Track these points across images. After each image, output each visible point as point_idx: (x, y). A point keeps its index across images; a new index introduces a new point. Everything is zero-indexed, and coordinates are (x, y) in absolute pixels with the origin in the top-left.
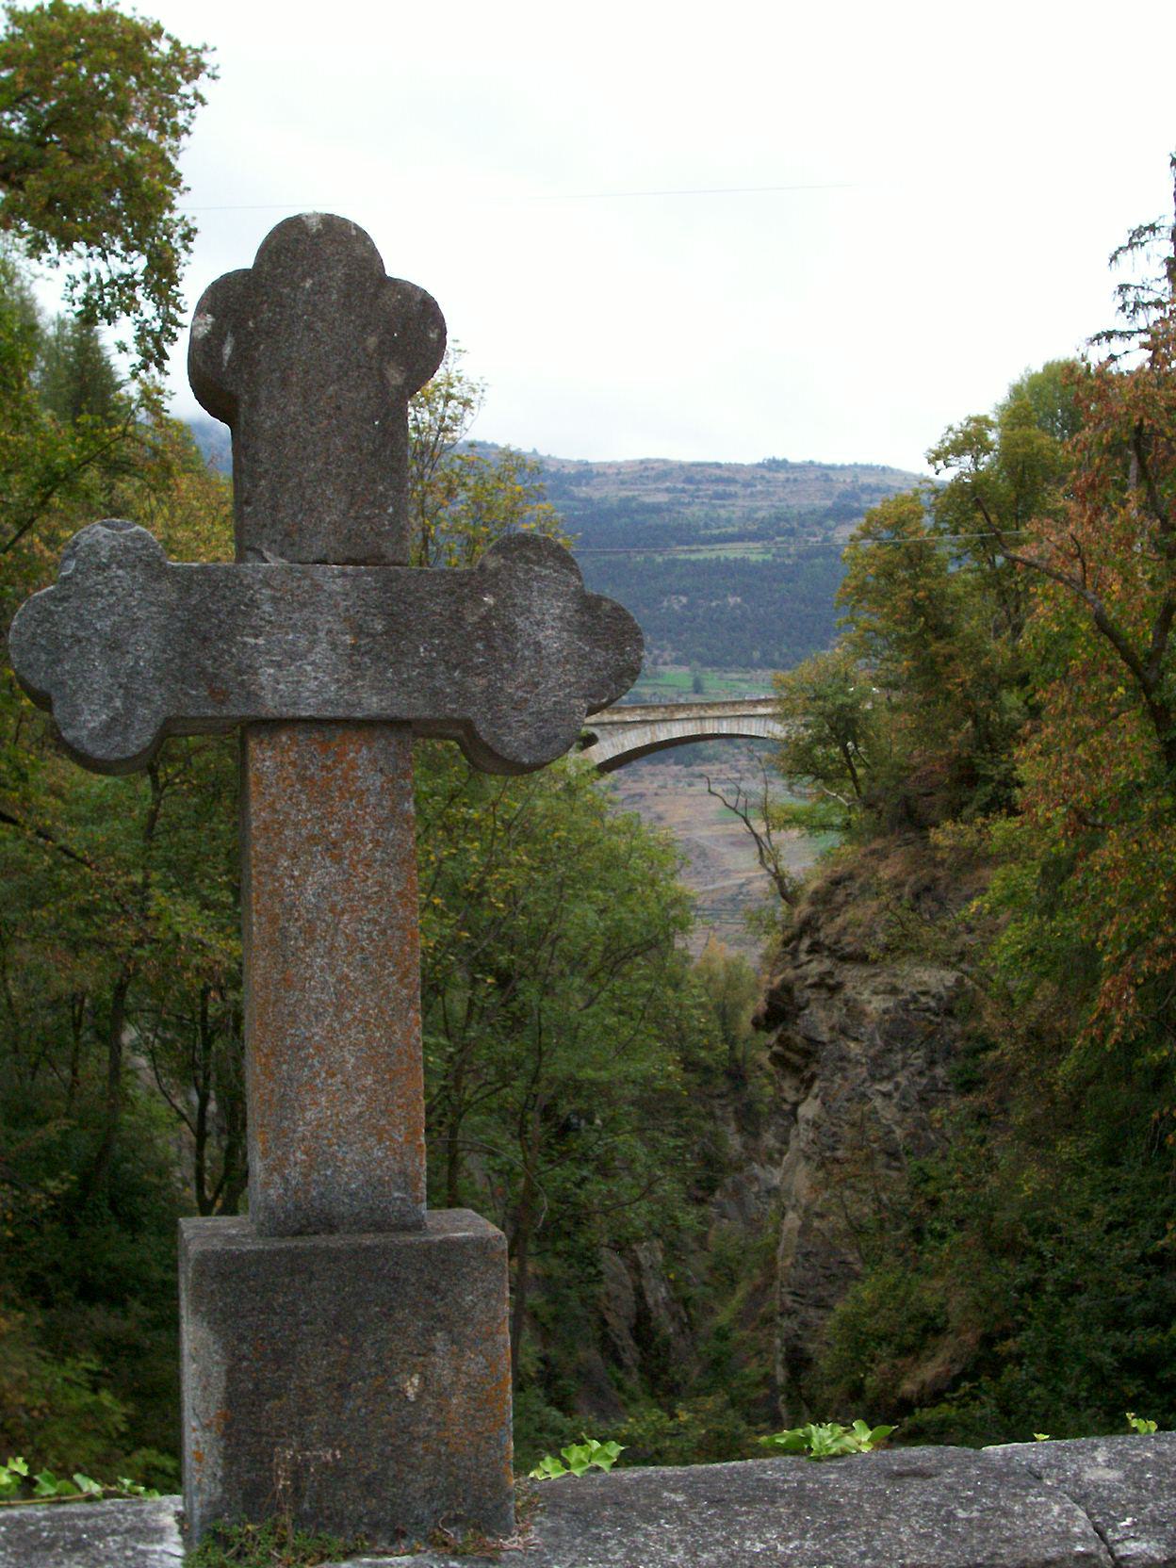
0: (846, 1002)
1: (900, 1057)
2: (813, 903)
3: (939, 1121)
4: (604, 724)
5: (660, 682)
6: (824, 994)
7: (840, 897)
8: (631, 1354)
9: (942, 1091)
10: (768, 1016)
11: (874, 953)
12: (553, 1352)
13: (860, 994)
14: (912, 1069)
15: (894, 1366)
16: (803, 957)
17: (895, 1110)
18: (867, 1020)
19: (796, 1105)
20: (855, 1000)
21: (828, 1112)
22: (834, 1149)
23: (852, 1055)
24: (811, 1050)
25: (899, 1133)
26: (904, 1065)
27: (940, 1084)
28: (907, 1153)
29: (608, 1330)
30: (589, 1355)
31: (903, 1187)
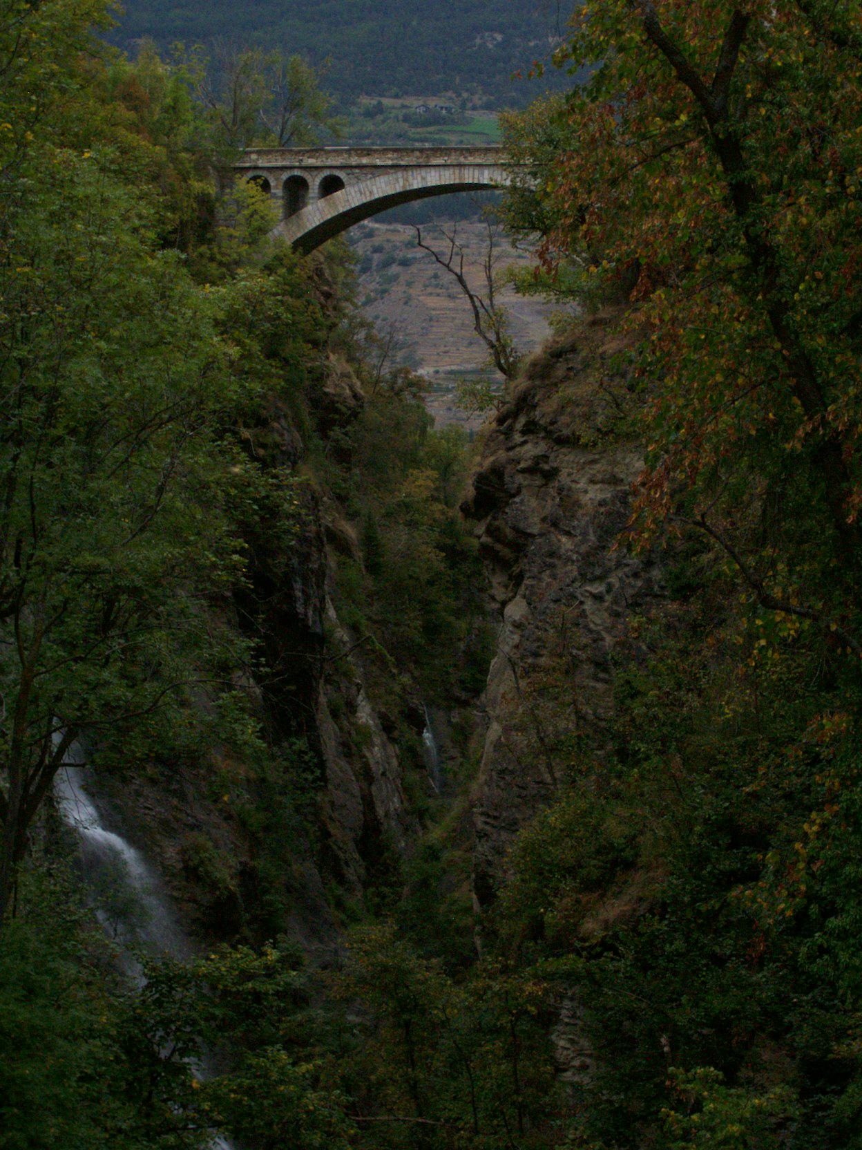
2: (531, 378)
4: (351, 167)
5: (469, 129)
6: (538, 480)
8: (354, 871)
9: (656, 596)
10: (477, 501)
11: (586, 437)
12: (259, 864)
14: (626, 569)
15: (578, 901)
16: (518, 438)
18: (580, 512)
19: (504, 604)
20: (570, 489)
22: (536, 655)
23: (563, 551)
24: (520, 542)
25: (609, 640)
26: (619, 565)
27: (656, 588)
28: (616, 664)
29: (330, 842)
30: (305, 869)
31: (610, 701)
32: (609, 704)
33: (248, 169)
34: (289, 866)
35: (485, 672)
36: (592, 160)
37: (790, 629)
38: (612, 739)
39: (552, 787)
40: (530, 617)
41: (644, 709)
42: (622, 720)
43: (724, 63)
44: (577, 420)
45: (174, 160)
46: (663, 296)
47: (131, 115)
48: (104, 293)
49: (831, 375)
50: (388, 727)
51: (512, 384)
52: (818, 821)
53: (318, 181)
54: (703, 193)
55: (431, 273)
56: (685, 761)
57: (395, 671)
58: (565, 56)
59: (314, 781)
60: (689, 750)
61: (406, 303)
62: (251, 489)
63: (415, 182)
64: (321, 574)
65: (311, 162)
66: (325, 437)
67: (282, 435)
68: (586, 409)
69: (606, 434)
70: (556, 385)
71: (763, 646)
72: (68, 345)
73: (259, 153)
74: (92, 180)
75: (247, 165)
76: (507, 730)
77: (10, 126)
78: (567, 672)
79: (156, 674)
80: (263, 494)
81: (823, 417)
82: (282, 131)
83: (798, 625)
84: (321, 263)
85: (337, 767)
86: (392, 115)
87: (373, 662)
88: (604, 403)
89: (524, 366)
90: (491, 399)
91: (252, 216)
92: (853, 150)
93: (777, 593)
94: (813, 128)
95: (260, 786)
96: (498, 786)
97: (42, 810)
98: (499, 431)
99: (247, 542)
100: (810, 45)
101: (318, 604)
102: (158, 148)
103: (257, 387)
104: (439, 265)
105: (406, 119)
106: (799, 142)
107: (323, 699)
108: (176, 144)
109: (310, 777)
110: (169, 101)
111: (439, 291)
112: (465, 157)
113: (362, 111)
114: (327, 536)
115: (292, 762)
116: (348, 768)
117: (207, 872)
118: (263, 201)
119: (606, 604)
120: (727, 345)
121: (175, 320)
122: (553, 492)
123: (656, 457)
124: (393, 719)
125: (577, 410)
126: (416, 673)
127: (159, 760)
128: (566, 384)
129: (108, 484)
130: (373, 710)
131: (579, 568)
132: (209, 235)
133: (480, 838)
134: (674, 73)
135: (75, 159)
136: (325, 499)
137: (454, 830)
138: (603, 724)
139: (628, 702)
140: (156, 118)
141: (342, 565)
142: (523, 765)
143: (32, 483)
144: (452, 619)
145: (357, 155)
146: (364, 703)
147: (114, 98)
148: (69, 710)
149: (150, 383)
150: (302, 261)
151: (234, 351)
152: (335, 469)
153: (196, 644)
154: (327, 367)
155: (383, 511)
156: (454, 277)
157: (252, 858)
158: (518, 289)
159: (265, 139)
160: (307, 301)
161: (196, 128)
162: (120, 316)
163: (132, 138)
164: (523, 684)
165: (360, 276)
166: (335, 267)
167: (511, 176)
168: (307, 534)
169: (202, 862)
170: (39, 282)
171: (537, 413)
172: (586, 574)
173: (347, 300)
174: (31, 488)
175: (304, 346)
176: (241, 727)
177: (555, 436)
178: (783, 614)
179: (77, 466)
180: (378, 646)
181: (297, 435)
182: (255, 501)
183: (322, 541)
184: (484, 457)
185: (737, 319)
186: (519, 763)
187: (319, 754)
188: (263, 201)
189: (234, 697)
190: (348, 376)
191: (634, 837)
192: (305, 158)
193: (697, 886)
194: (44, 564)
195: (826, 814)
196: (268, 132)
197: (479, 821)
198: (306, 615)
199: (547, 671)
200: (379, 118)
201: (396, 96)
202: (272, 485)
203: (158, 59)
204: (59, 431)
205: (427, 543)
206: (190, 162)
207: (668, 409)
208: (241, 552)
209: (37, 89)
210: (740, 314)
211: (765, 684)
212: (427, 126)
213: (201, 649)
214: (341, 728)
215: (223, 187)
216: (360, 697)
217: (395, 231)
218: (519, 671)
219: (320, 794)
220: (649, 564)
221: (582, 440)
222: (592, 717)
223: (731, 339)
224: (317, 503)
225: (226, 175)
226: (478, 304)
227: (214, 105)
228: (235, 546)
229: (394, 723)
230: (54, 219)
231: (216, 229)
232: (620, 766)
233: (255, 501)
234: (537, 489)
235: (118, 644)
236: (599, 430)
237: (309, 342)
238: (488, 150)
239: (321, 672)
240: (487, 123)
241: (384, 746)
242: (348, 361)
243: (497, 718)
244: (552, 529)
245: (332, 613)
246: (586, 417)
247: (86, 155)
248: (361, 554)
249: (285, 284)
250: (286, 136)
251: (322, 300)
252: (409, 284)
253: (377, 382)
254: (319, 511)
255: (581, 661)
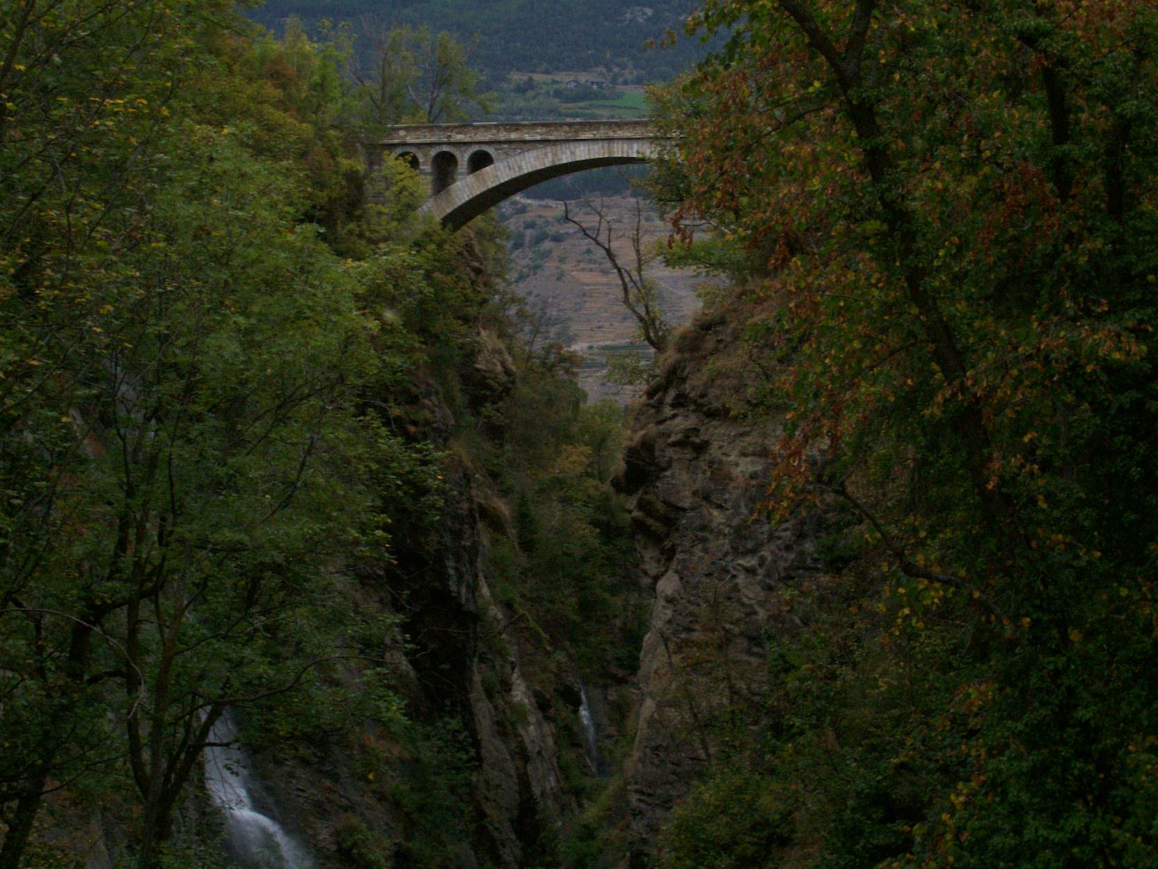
0: (711, 463)
1: (766, 528)
2: (680, 350)
3: (787, 604)
4: (500, 142)
6: (689, 454)
7: (710, 344)
9: (807, 569)
12: (414, 846)
13: (727, 455)
14: (779, 542)
16: (668, 411)
17: (759, 589)
18: (732, 485)
19: (656, 578)
20: (721, 462)
21: (685, 588)
22: (689, 630)
23: (714, 524)
24: (671, 516)
25: (762, 614)
26: (771, 538)
27: (809, 561)
28: (770, 637)
32: (764, 679)
33: (395, 145)
34: (445, 846)
35: (639, 649)
36: (724, 127)
37: (933, 598)
38: (766, 714)
39: (706, 764)
40: (682, 591)
41: (797, 683)
42: (775, 695)
43: (856, 29)
44: (727, 392)
45: (321, 136)
46: (799, 263)
47: (278, 93)
48: (243, 268)
49: (971, 340)
50: (543, 705)
51: (662, 358)
52: (965, 791)
53: (467, 156)
54: (838, 159)
55: (584, 248)
56: (838, 736)
57: (549, 648)
58: (698, 24)
59: (469, 761)
60: (844, 723)
61: (559, 279)
62: (395, 464)
63: (564, 156)
64: (474, 551)
65: (459, 137)
66: (477, 413)
67: (433, 412)
68: (735, 381)
69: (756, 405)
70: (705, 357)
71: (907, 615)
72: (206, 320)
73: (407, 129)
74: (230, 155)
75: (396, 141)
76: (660, 706)
77: (145, 102)
78: (720, 647)
79: (299, 651)
80: (407, 469)
81: (962, 383)
82: (431, 107)
83: (941, 593)
84: (471, 239)
85: (493, 746)
86: (543, 91)
87: (527, 640)
88: (753, 375)
89: (673, 339)
90: (641, 372)
91: (400, 192)
92: (989, 116)
93: (920, 559)
94: (950, 94)
95: (414, 767)
96: (652, 763)
97: (189, 789)
98: (649, 405)
99: (390, 518)
100: (943, 10)
101: (471, 581)
102: (304, 125)
103: (398, 361)
104: (588, 241)
105: (557, 94)
106: (935, 108)
107: (477, 678)
108: (323, 121)
109: (465, 757)
110: (316, 78)
111: (591, 266)
112: (614, 132)
113: (512, 86)
114: (480, 514)
115: (447, 742)
116: (503, 747)
117: (361, 855)
118: (411, 177)
119: (759, 577)
120: (865, 312)
121: (314, 295)
122: (704, 465)
123: (795, 426)
124: (548, 697)
125: (727, 382)
126: (572, 651)
127: (309, 739)
128: (716, 356)
129: (247, 459)
130: (528, 688)
131: (731, 542)
132: (358, 213)
133: (634, 815)
134: (807, 40)
135: (214, 135)
136: (477, 476)
137: (610, 809)
138: (756, 699)
139: (782, 676)
140: (303, 95)
141: (495, 542)
142: (677, 741)
143: (170, 459)
144: (607, 595)
145: (506, 130)
146: (518, 682)
147: (260, 76)
148: (209, 688)
149: (289, 358)
150: (452, 237)
151: (373, 325)
152: (488, 446)
153: (340, 622)
154: (478, 343)
155: (536, 488)
156: (604, 252)
157: (409, 838)
158: (668, 263)
159: (414, 115)
160: (457, 277)
161: (344, 105)
162: (258, 291)
163: (278, 116)
164: (676, 659)
165: (511, 252)
166: (485, 243)
167: (659, 149)
168: (460, 512)
169: (355, 844)
170: (174, 257)
171: (687, 386)
172: (737, 548)
173: (498, 276)
174: (169, 462)
175: (455, 321)
176: (385, 704)
177: (705, 409)
178: (926, 582)
179: (215, 441)
180: (532, 624)
181: (448, 412)
182: (399, 475)
183: (473, 517)
184: (634, 431)
185: (875, 286)
186: (673, 739)
187: (474, 734)
188: (411, 177)
189: (378, 674)
190: (500, 352)
191: (790, 813)
192: (453, 134)
193: (851, 861)
194: (181, 541)
195: (973, 784)
196: (417, 108)
197: (634, 798)
198: (459, 593)
199: (699, 645)
200: (530, 93)
201: (547, 72)
202: (416, 460)
203: (305, 37)
204: (198, 409)
205: (581, 519)
206: (338, 139)
207: (806, 376)
208: (386, 528)
209: (170, 64)
210: (879, 280)
211: (920, 656)
212: (579, 101)
213: (346, 625)
214: (496, 708)
215: (371, 164)
216: (515, 676)
217: (547, 207)
218: (672, 646)
219: (475, 774)
220: (801, 536)
221: (732, 413)
222: (745, 692)
223: (868, 305)
224: (469, 482)
225: (375, 152)
226: (627, 280)
227: (362, 82)
228: (377, 522)
229: (549, 701)
230: (194, 194)
231: (365, 206)
232: (774, 741)
233: (399, 475)
234: (688, 463)
235: (259, 621)
236: (748, 402)
237: (459, 318)
238: (637, 124)
239: (475, 651)
240: (635, 98)
241: (539, 724)
242: (499, 337)
243: (651, 694)
244: (704, 503)
245: (485, 591)
246: (737, 389)
247: (226, 131)
248: (514, 531)
249: (435, 260)
250: (436, 111)
251: (473, 275)
252: (562, 260)
253: (529, 358)
254: (471, 488)
255: (735, 636)
